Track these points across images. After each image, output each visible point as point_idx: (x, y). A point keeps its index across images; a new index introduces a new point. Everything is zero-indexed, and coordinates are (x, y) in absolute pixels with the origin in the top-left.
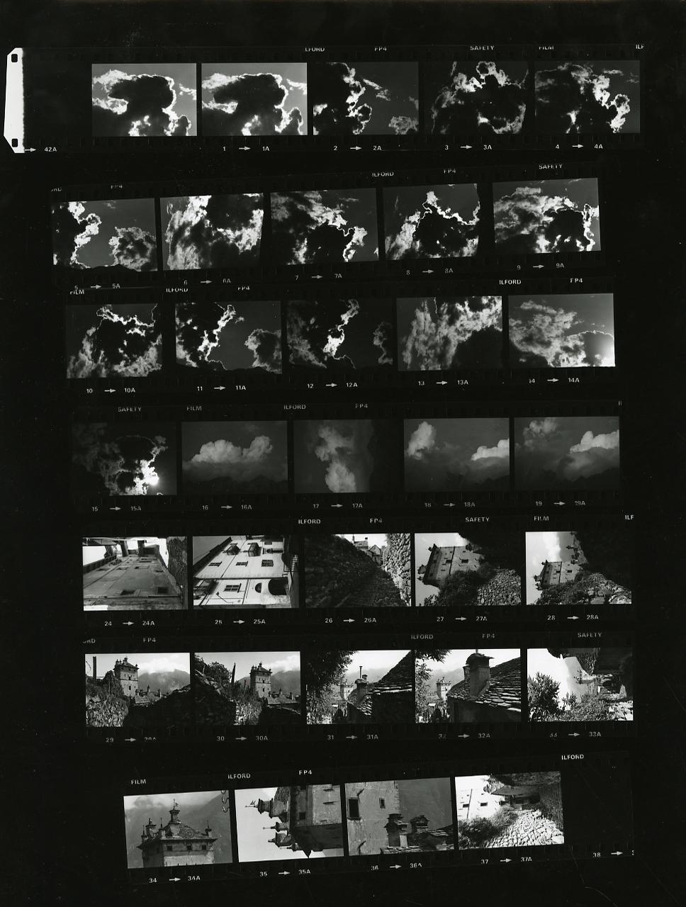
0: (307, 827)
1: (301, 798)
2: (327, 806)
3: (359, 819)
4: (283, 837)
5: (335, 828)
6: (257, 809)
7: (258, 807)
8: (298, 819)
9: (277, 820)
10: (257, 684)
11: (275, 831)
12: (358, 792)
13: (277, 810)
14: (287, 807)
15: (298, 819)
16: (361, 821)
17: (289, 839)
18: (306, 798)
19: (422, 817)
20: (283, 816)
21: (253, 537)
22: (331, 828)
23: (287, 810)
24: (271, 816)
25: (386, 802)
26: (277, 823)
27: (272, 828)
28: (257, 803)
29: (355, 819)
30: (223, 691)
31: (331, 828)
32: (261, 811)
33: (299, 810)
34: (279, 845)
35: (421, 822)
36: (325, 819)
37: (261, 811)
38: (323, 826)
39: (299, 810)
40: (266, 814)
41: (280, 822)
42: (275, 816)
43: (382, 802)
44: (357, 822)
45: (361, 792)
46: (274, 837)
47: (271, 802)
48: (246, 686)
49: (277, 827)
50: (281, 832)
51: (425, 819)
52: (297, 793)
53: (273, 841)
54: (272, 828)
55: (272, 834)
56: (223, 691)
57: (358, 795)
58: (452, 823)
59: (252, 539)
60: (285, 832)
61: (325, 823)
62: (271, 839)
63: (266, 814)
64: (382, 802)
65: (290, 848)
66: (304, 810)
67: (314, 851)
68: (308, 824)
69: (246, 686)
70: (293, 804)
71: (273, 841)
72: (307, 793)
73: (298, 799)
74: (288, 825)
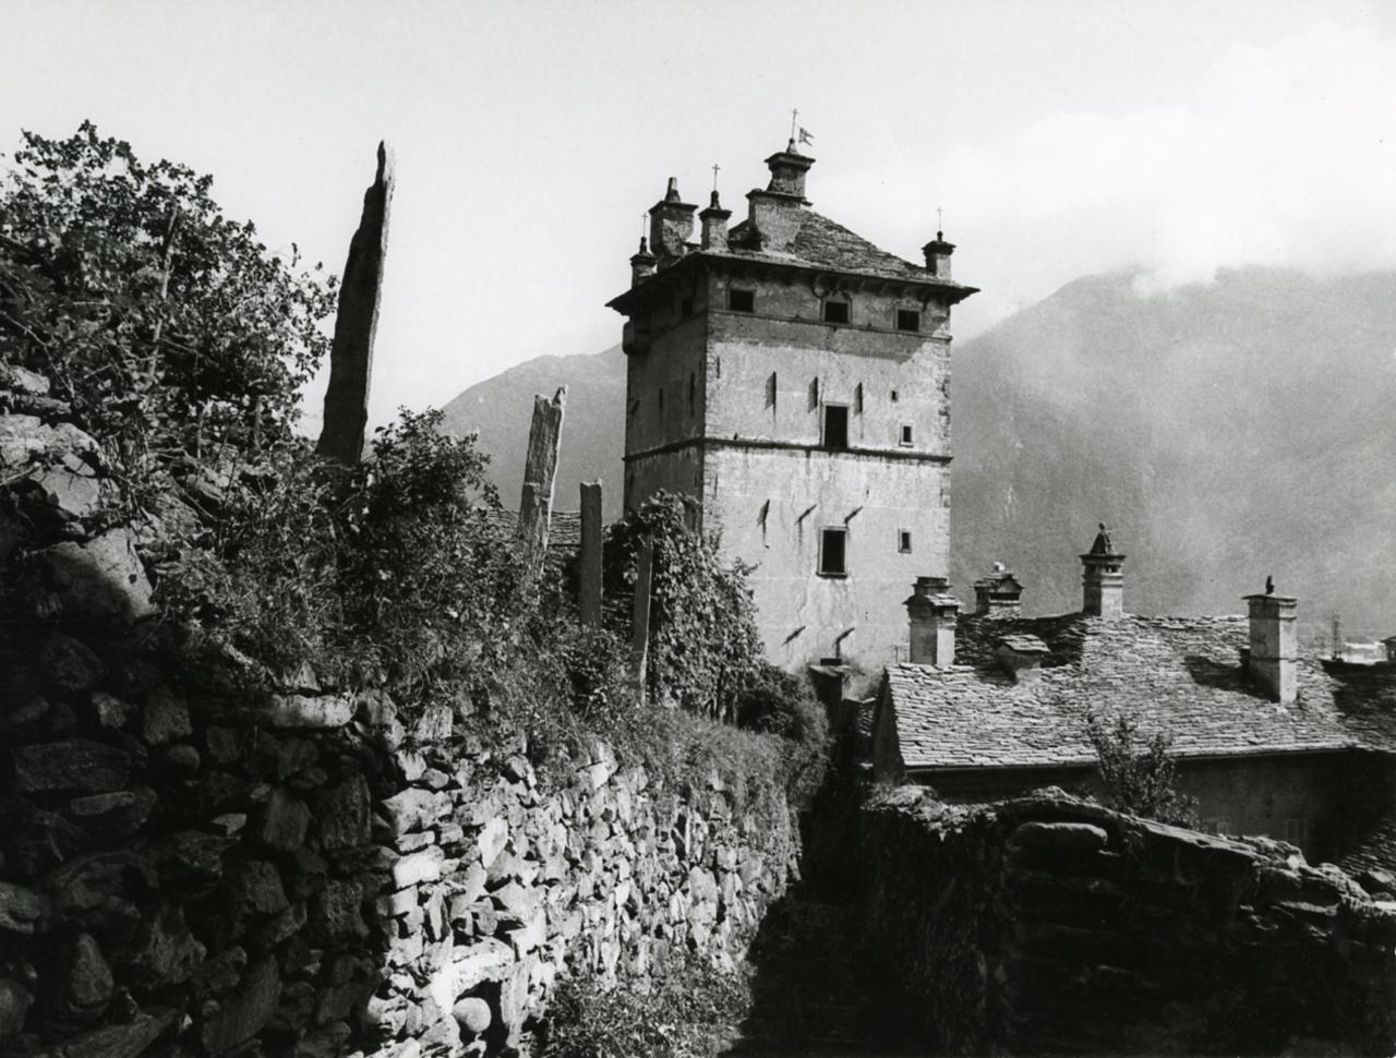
0: (705, 313)
1: (802, 301)
2: (764, 383)
3: (844, 577)
4: (681, 230)
5: (691, 399)
6: (784, 150)
7: (789, 154)
8: (736, 285)
9: (739, 215)
10: (722, 463)
11: (704, 204)
12: (848, 514)
13: (772, 221)
14: (775, 253)
15: (736, 285)
16: (849, 581)
17: (672, 246)
18: (797, 320)
19: (1008, 579)
20: (749, 236)
21: (1245, 837)
22: (692, 388)
23: (766, 251)
24: (754, 196)
25: (913, 540)
26: (726, 215)
27: (715, 196)
28: (802, 150)
29: (834, 577)
30: (198, 568)
31: (692, 388)
32: (776, 163)
33: (761, 292)
34: (658, 213)
35: (1002, 590)
36: (724, 376)
37: (776, 163)
38: (703, 366)
39: (761, 292)
40: (763, 179)
41: (732, 223)
42: (752, 210)
43: (906, 537)
44: (838, 582)
45: (854, 514)
46: (685, 199)
47: (800, 200)
48: (561, 497)
49: (715, 214)
50: (698, 224)
51: (1013, 581)
52: (819, 291)
53: (672, 193)
54: (715, 196)
55: (695, 195)
56: (198, 568)
57: (847, 520)
58: (907, 763)
59: (1241, 840)
60: (695, 238)
61: (710, 373)
62: (679, 187)
63: (763, 179)
64: (906, 537)
65: (643, 248)
66: (759, 309)
67: (626, 327)
68: (714, 319)
69: (561, 497)
70: (785, 275)
71: (672, 193)
72: (813, 322)
73: (799, 290)
74: (718, 249)
